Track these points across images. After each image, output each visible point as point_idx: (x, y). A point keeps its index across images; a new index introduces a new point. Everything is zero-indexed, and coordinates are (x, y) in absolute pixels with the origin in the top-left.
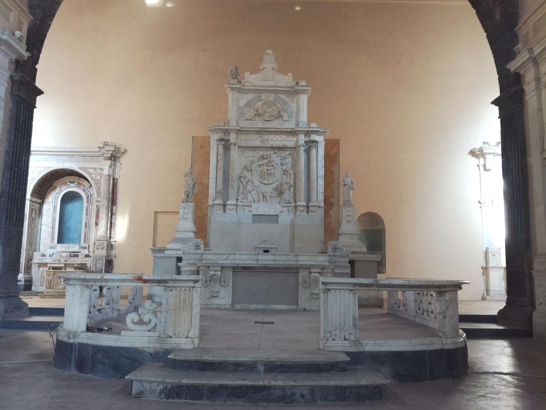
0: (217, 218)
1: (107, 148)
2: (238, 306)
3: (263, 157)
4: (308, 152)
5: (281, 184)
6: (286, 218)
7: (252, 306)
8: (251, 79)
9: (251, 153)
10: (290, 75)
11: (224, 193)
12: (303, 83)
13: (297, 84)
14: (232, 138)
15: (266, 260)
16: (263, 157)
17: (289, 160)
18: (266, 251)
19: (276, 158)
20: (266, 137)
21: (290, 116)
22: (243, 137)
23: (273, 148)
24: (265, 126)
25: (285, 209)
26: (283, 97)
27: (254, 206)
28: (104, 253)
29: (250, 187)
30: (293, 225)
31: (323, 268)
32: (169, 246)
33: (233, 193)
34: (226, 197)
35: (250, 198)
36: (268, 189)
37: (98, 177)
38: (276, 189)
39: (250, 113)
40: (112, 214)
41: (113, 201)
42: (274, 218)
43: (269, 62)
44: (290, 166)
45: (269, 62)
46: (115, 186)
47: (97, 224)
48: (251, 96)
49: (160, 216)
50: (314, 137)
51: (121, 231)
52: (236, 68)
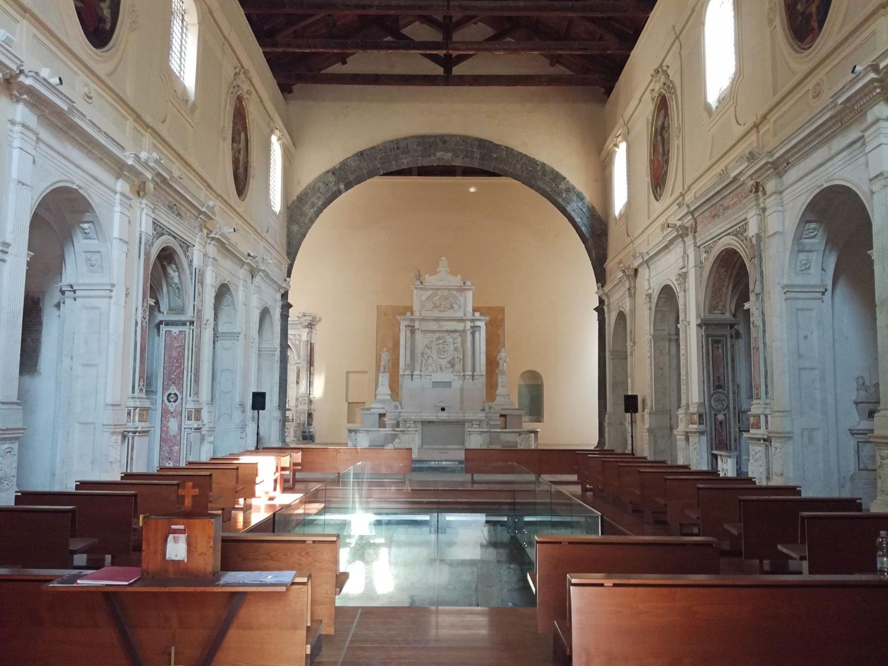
0: (406, 384)
1: (305, 318)
2: (425, 447)
3: (439, 338)
4: (473, 334)
5: (453, 358)
6: (457, 384)
7: (435, 447)
8: (429, 279)
9: (430, 335)
10: (459, 276)
11: (412, 366)
12: (468, 283)
13: (464, 283)
14: (417, 325)
15: (443, 416)
16: (439, 338)
17: (459, 340)
18: (443, 409)
19: (449, 339)
20: (442, 323)
21: (460, 307)
22: (424, 323)
23: (447, 331)
24: (441, 315)
25: (456, 378)
26: (454, 292)
27: (433, 375)
28: (306, 407)
29: (430, 361)
30: (462, 390)
31: (481, 421)
32: (373, 406)
33: (417, 365)
34: (413, 370)
35: (430, 369)
36: (444, 362)
37: (297, 342)
38: (449, 362)
39: (429, 305)
40: (310, 374)
41: (311, 363)
42: (448, 384)
43: (443, 267)
44: (459, 344)
45: (443, 267)
46: (312, 349)
47: (298, 383)
48: (430, 293)
49: (351, 376)
50: (478, 323)
51: (318, 389)
52: (419, 271)
